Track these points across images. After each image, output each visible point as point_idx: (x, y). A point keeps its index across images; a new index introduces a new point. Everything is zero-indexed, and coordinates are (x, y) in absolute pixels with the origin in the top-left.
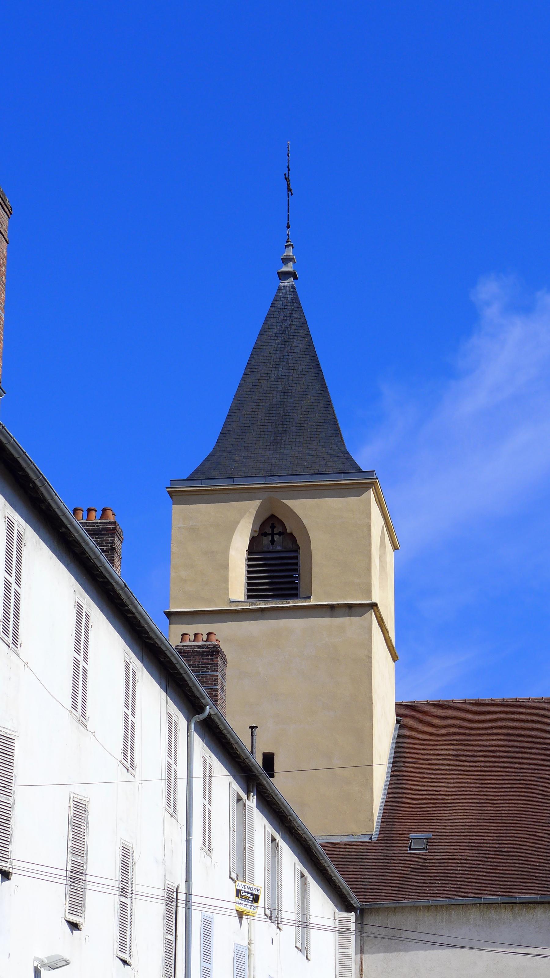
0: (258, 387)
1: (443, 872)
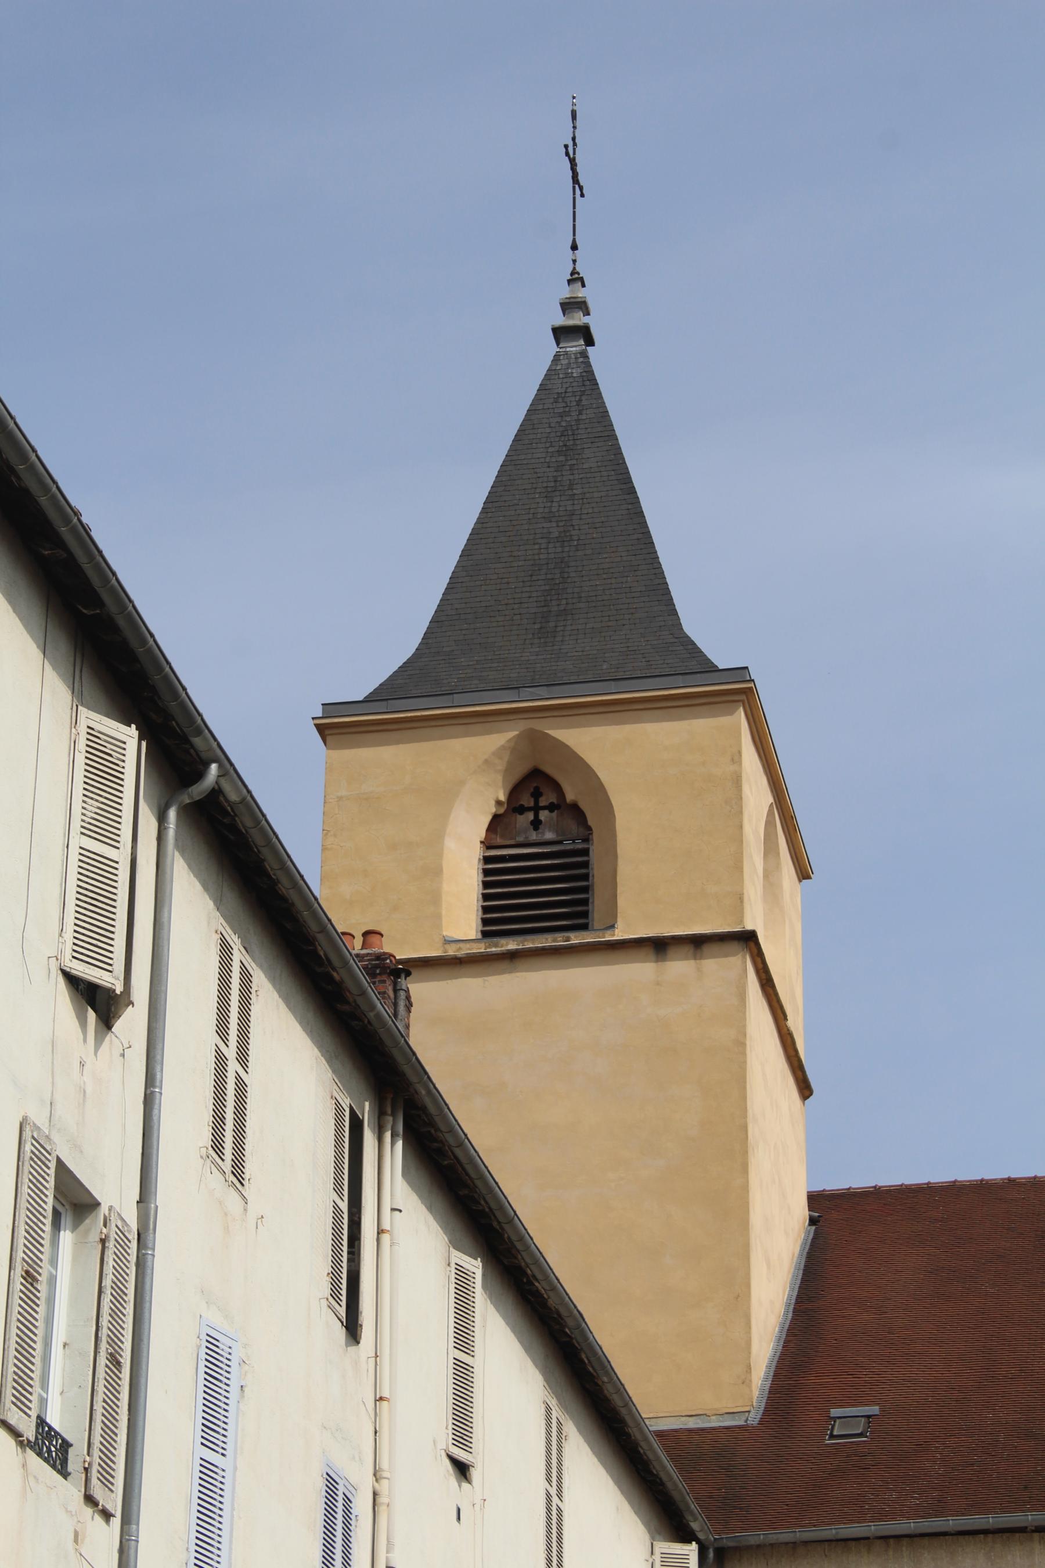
0: (508, 534)
1: (901, 1474)
